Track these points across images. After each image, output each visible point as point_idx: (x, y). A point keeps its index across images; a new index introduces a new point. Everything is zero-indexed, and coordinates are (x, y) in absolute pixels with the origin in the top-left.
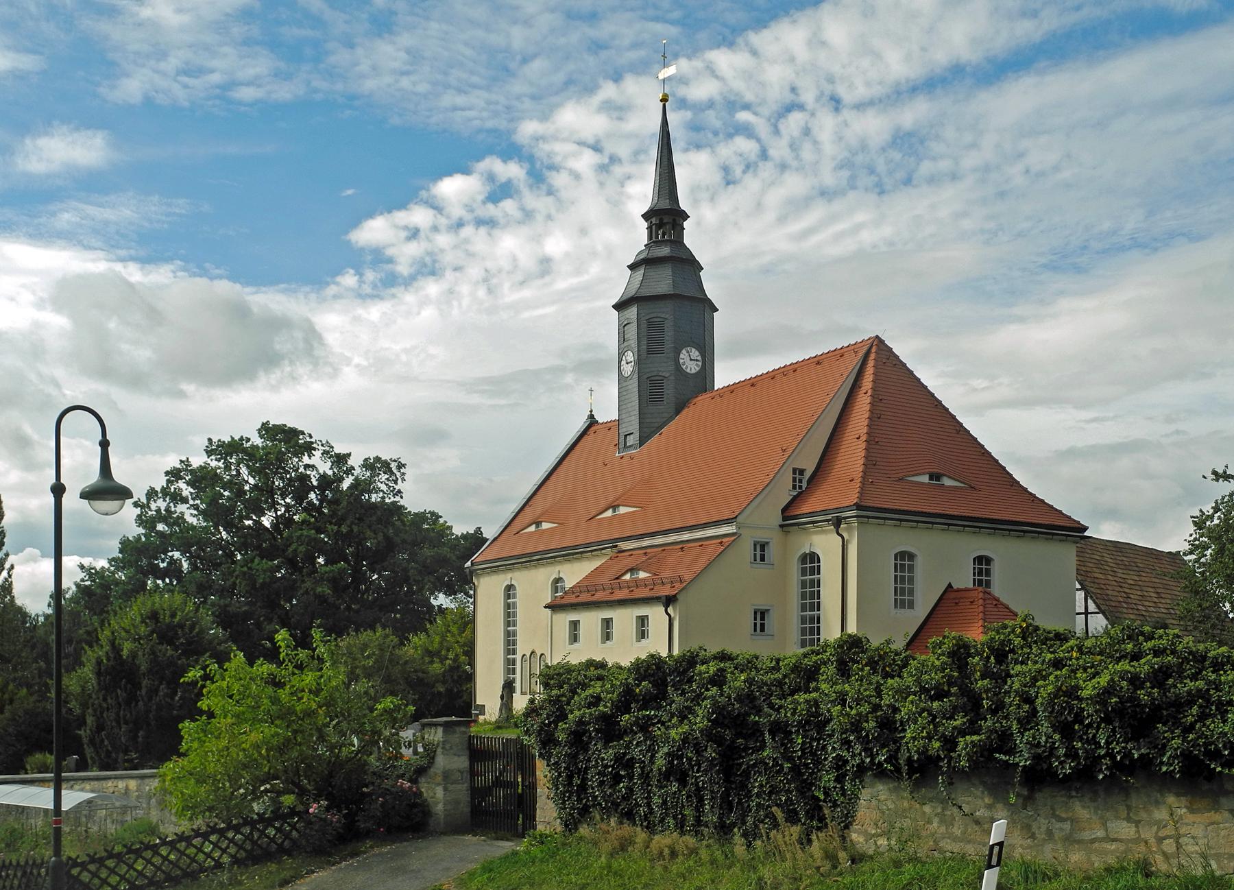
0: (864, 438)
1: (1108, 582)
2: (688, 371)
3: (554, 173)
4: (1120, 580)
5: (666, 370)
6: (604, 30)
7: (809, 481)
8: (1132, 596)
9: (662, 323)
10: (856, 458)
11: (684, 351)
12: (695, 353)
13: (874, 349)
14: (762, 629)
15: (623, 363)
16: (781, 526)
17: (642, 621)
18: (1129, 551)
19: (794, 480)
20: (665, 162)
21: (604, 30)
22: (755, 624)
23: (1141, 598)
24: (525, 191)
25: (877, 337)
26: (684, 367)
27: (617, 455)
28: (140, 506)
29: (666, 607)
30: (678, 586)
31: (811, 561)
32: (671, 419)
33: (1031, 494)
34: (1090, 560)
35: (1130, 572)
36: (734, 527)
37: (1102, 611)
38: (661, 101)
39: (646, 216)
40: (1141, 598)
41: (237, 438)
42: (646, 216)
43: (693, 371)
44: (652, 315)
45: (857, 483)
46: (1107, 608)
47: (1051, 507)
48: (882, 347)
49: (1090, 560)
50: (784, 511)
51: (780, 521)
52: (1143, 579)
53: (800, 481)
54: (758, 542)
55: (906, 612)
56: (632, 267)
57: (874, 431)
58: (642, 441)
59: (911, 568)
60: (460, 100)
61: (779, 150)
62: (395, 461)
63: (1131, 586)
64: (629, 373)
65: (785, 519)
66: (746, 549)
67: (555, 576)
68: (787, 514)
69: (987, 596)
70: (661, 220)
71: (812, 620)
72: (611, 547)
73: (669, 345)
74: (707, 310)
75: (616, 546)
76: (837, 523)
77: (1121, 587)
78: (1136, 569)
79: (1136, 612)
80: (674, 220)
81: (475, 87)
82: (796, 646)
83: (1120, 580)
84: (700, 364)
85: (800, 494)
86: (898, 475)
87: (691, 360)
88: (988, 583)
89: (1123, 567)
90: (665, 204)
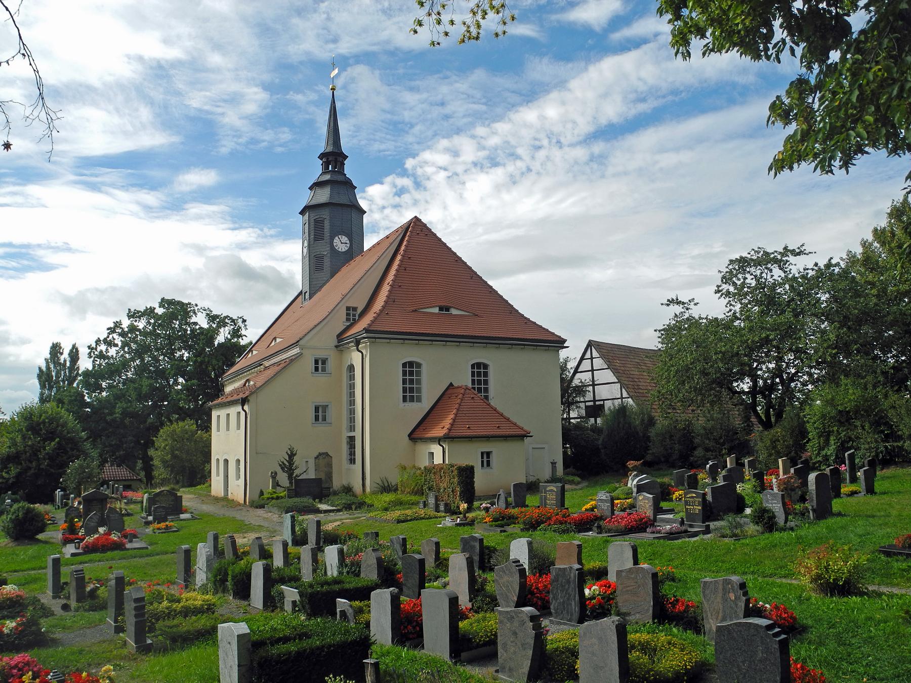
2: (340, 250)
3: (428, 181)
5: (324, 250)
6: (448, 110)
9: (323, 221)
11: (337, 238)
12: (345, 239)
16: (336, 347)
19: (348, 314)
21: (448, 110)
24: (413, 191)
25: (416, 217)
26: (337, 248)
31: (351, 368)
32: (328, 281)
33: (526, 318)
39: (321, 156)
41: (149, 307)
42: (321, 156)
43: (343, 250)
47: (541, 327)
48: (418, 223)
50: (339, 336)
53: (354, 315)
55: (415, 405)
60: (383, 147)
61: (536, 166)
62: (240, 318)
70: (328, 159)
73: (327, 234)
74: (354, 215)
80: (336, 159)
81: (389, 140)
84: (348, 245)
86: (412, 308)
87: (342, 243)
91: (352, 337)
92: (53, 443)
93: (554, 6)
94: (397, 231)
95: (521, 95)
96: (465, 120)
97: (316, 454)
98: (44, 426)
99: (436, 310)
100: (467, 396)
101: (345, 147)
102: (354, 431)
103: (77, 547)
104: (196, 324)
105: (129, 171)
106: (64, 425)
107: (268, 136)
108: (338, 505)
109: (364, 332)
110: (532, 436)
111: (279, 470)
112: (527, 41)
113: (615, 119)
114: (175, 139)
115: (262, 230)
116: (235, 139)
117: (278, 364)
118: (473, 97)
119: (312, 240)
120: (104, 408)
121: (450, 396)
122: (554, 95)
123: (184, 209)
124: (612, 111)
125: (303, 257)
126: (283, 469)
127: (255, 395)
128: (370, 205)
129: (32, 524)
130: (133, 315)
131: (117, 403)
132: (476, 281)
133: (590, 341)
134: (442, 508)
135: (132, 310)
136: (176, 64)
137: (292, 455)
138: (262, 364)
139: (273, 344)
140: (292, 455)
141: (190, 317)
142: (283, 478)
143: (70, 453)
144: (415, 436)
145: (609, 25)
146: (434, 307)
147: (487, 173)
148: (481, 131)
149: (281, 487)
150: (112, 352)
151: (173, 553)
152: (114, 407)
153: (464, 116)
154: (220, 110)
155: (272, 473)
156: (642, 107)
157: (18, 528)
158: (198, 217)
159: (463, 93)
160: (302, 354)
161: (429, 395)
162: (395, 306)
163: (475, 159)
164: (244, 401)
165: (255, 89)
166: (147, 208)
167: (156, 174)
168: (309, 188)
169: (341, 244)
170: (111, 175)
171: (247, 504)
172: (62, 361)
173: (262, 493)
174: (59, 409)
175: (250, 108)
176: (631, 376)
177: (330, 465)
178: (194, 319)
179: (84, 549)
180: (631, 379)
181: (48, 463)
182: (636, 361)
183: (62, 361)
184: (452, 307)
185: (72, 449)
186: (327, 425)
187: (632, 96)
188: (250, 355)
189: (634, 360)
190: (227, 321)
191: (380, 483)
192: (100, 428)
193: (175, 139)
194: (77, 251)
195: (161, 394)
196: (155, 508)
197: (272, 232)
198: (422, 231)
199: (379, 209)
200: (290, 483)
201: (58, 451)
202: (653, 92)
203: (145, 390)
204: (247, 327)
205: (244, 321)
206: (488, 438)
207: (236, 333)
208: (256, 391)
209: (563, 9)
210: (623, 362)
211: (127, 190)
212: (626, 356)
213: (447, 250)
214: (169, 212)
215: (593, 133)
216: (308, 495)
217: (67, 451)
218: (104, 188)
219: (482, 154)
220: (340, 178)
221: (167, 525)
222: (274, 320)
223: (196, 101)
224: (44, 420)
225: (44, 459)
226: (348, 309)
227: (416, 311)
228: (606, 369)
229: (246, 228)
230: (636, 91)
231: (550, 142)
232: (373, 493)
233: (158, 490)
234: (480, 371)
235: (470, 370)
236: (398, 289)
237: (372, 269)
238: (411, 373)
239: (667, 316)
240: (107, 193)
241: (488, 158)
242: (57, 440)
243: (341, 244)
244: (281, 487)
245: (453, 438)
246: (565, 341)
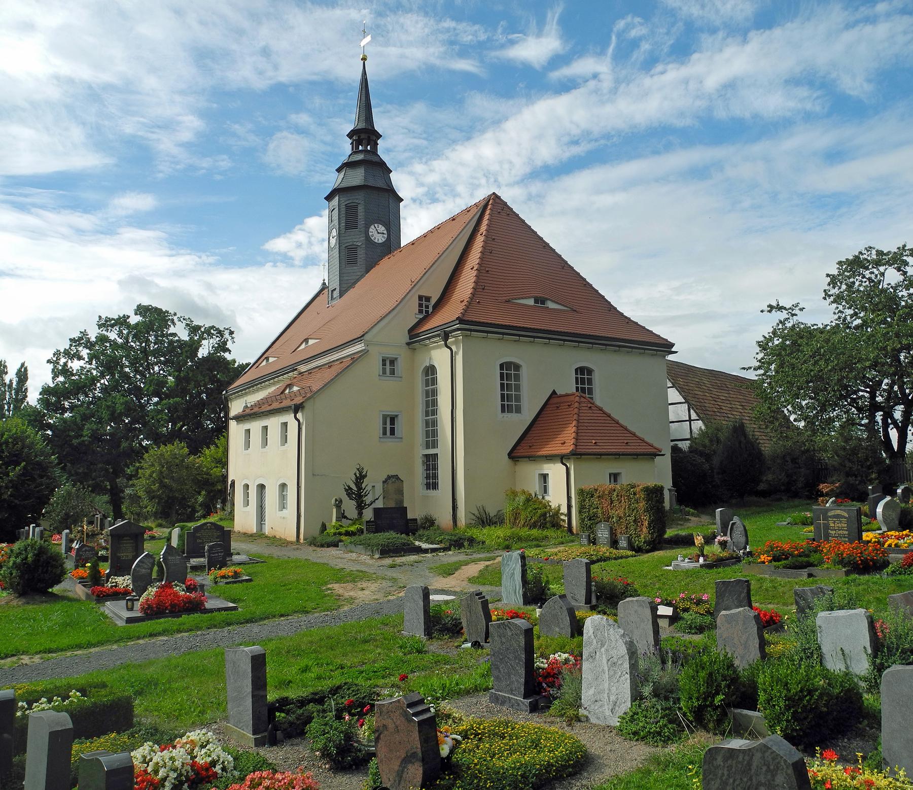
1: (705, 397)
2: (376, 241)
4: (715, 396)
5: (359, 240)
8: (723, 408)
9: (356, 207)
12: (382, 228)
15: (331, 237)
16: (408, 344)
18: (721, 377)
19: (420, 305)
20: (364, 98)
23: (731, 409)
25: (494, 193)
26: (373, 238)
28: (51, 362)
29: (296, 412)
31: (431, 370)
32: (362, 276)
34: (691, 382)
35: (722, 391)
36: (363, 345)
37: (700, 418)
38: (362, 60)
40: (731, 409)
41: (122, 316)
42: (350, 135)
43: (380, 241)
46: (704, 416)
48: (498, 200)
49: (691, 382)
50: (411, 331)
52: (732, 396)
53: (427, 307)
54: (388, 358)
55: (513, 416)
58: (341, 296)
59: (517, 377)
60: (324, 178)
62: (227, 329)
63: (723, 401)
69: (582, 399)
73: (361, 222)
76: (446, 337)
77: (715, 401)
78: (727, 389)
79: (726, 419)
82: (421, 448)
83: (715, 396)
84: (386, 236)
86: (505, 298)
87: (378, 233)
88: (590, 391)
89: (716, 387)
91: (440, 328)
92: (18, 468)
93: (494, 43)
94: (468, 210)
95: (461, 131)
96: (407, 154)
97: (384, 477)
98: (7, 446)
99: (531, 302)
100: (584, 405)
103: (130, 607)
104: (175, 335)
105: (61, 192)
106: (31, 446)
107: (206, 163)
108: (441, 542)
109: (457, 322)
110: (663, 455)
111: (345, 498)
112: (467, 76)
113: (550, 161)
114: (109, 161)
115: (200, 257)
116: (173, 166)
117: (330, 365)
118: (414, 132)
119: (343, 228)
120: (69, 430)
122: (489, 135)
123: (118, 234)
124: (548, 152)
125: (330, 249)
126: (349, 495)
127: (312, 400)
128: (309, 237)
129: (47, 571)
130: (106, 323)
131: (85, 424)
132: (568, 271)
134: (623, 543)
135: (104, 317)
136: (108, 88)
137: (360, 478)
138: (296, 369)
139: (303, 346)
140: (360, 478)
141: (168, 327)
142: (350, 507)
143: (39, 480)
145: (549, 63)
146: (529, 298)
147: (428, 208)
148: (419, 168)
149: (347, 519)
150: (75, 365)
151: (282, 616)
152: (81, 429)
153: (405, 151)
154: (154, 136)
155: (336, 500)
156: (576, 150)
157: (26, 577)
158: (134, 242)
159: (403, 128)
160: (368, 351)
161: (530, 407)
162: (486, 294)
163: (414, 195)
164: (297, 409)
165: (191, 118)
166: (80, 232)
167: (91, 196)
168: (325, 198)
169: (378, 234)
170: (42, 196)
171: (302, 541)
172: (7, 382)
173: (324, 527)
174: (25, 427)
175: (186, 136)
177: (400, 492)
178: (172, 330)
179: (143, 609)
181: (11, 492)
182: (697, 380)
183: (7, 382)
185: (41, 477)
186: (396, 440)
187: (566, 139)
188: (264, 363)
189: (693, 379)
190: (212, 331)
191: (476, 513)
192: (64, 453)
193: (109, 161)
195: (138, 413)
196: (210, 547)
197: (212, 259)
198: (502, 210)
199: (319, 242)
200: (359, 513)
201: (23, 478)
202: (587, 135)
203: (119, 408)
204: (235, 340)
205: (231, 333)
206: (617, 456)
207: (223, 347)
208: (312, 396)
209: (502, 46)
210: (686, 381)
211: (59, 213)
212: (686, 375)
213: (533, 234)
214: (102, 236)
215: (530, 174)
216: (391, 529)
217: (34, 478)
218: (33, 210)
219: (421, 190)
220: (374, 159)
221: (235, 572)
223: (129, 127)
224: (6, 439)
225: (7, 487)
226: (420, 298)
228: (671, 387)
229: (182, 254)
230: (569, 134)
231: (488, 181)
232: (469, 526)
233: (199, 523)
234: (584, 374)
236: (485, 275)
237: (448, 251)
238: (509, 377)
239: (766, 326)
240: (37, 215)
241: (426, 195)
242: (23, 464)
243: (378, 234)
244: (347, 519)
245: (581, 455)
246: (672, 345)
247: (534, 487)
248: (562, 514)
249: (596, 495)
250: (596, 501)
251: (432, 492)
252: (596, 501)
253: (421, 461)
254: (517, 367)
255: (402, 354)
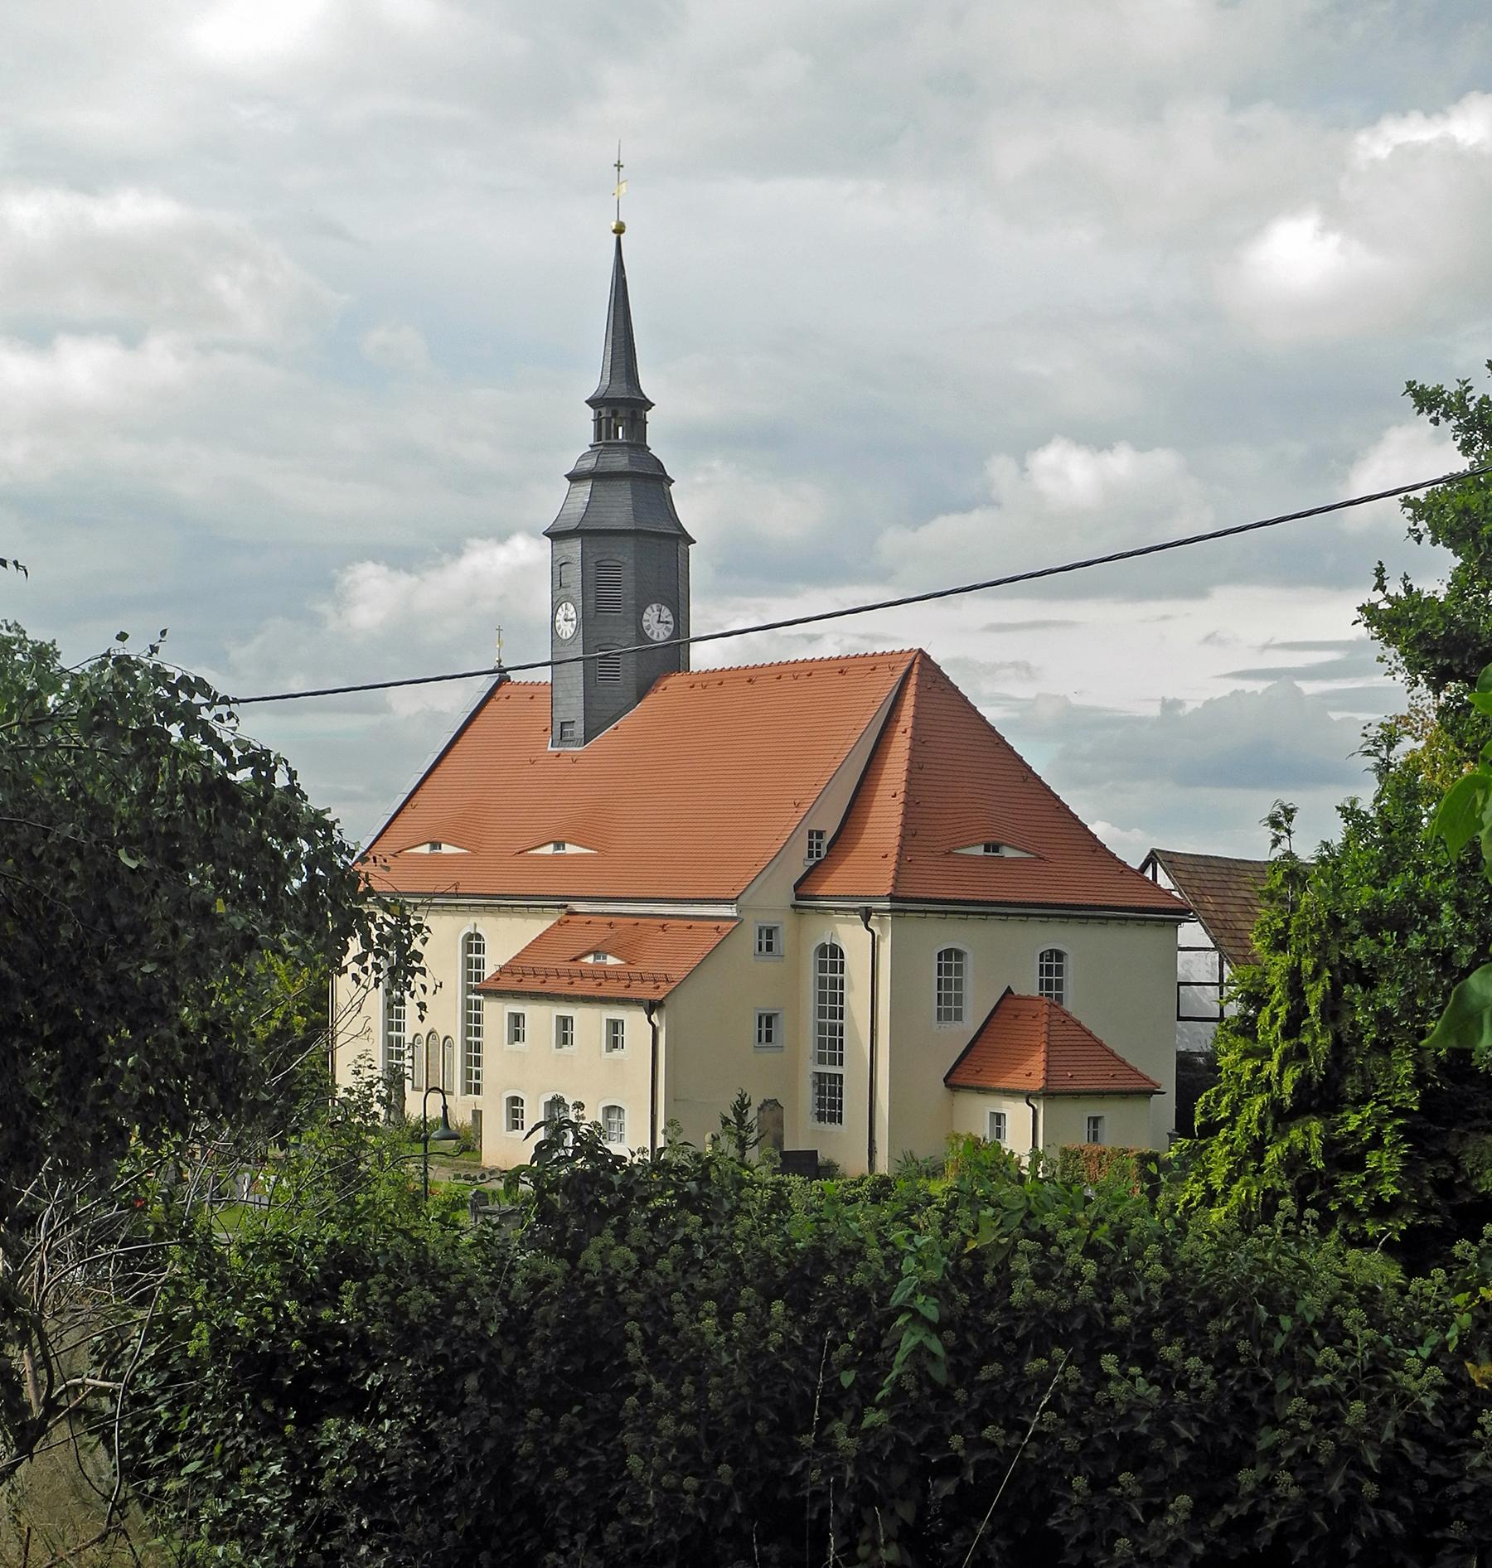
0: (901, 797)
7: (829, 847)
10: (889, 825)
12: (666, 613)
13: (915, 670)
14: (769, 1039)
16: (794, 906)
17: (615, 1026)
19: (811, 845)
20: (621, 325)
22: (760, 1032)
26: (648, 633)
27: (550, 749)
30: (665, 988)
31: (831, 956)
33: (1120, 861)
38: (614, 231)
44: (599, 559)
45: (891, 863)
50: (797, 887)
51: (793, 900)
53: (818, 846)
55: (953, 1027)
56: (574, 477)
57: (916, 787)
59: (959, 969)
64: (569, 635)
65: (798, 898)
66: (749, 938)
67: (469, 929)
68: (800, 892)
71: (833, 1030)
72: (558, 907)
75: (566, 906)
80: (633, 413)
84: (671, 626)
85: (818, 862)
90: (621, 391)
100: (1055, 1018)
101: (648, 385)
102: (841, 1064)
121: (1016, 1013)
133: (1153, 852)
137: (741, 1107)
144: (958, 1080)
176: (1239, 934)
180: (1239, 943)
184: (1003, 844)
194: (1220, 677)
206: (1101, 1095)
222: (444, 764)
227: (950, 853)
234: (1052, 963)
235: (1038, 963)
247: (984, 1130)
248: (1023, 1168)
249: (1082, 1156)
250: (1082, 1163)
251: (828, 1127)
252: (1082, 1163)
253: (810, 1081)
254: (960, 955)
255: (784, 921)
